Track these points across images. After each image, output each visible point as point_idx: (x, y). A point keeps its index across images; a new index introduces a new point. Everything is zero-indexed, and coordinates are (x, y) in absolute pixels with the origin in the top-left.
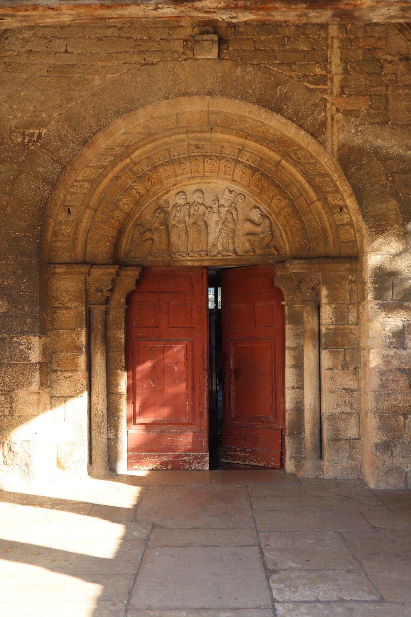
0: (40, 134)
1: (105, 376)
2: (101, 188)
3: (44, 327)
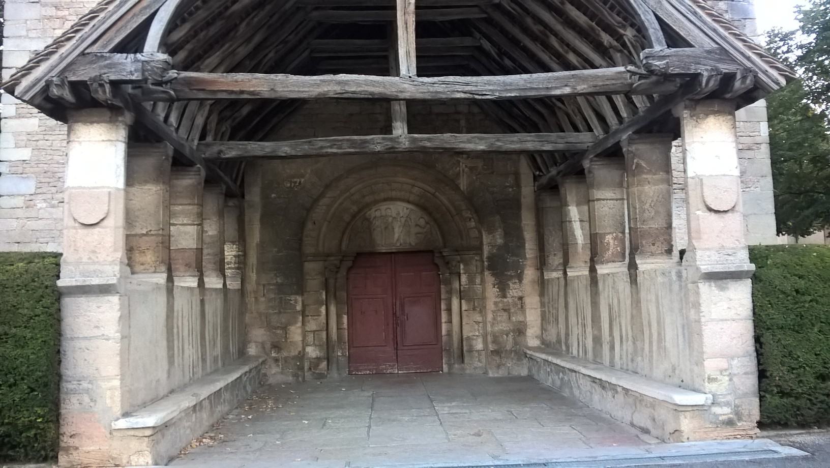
0: (300, 183)
1: (68, 347)
2: (333, 210)
3: (301, 290)
